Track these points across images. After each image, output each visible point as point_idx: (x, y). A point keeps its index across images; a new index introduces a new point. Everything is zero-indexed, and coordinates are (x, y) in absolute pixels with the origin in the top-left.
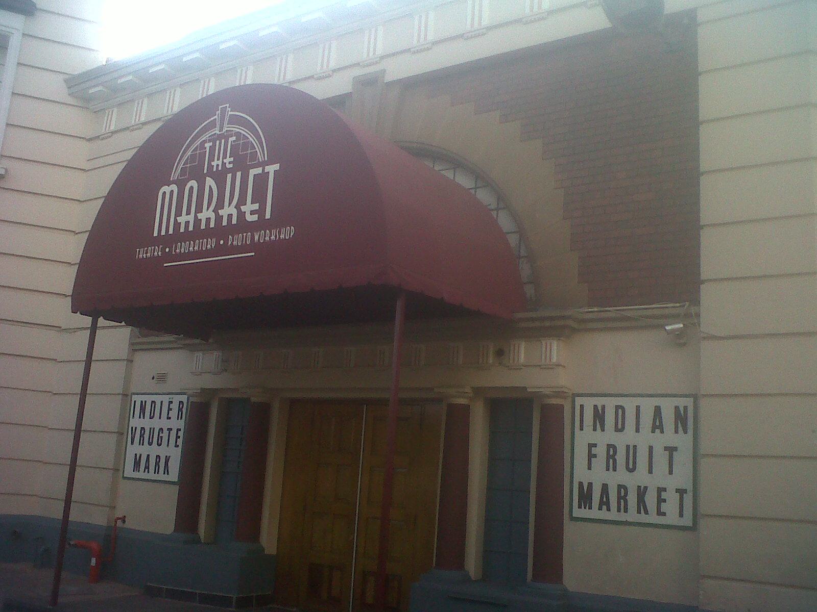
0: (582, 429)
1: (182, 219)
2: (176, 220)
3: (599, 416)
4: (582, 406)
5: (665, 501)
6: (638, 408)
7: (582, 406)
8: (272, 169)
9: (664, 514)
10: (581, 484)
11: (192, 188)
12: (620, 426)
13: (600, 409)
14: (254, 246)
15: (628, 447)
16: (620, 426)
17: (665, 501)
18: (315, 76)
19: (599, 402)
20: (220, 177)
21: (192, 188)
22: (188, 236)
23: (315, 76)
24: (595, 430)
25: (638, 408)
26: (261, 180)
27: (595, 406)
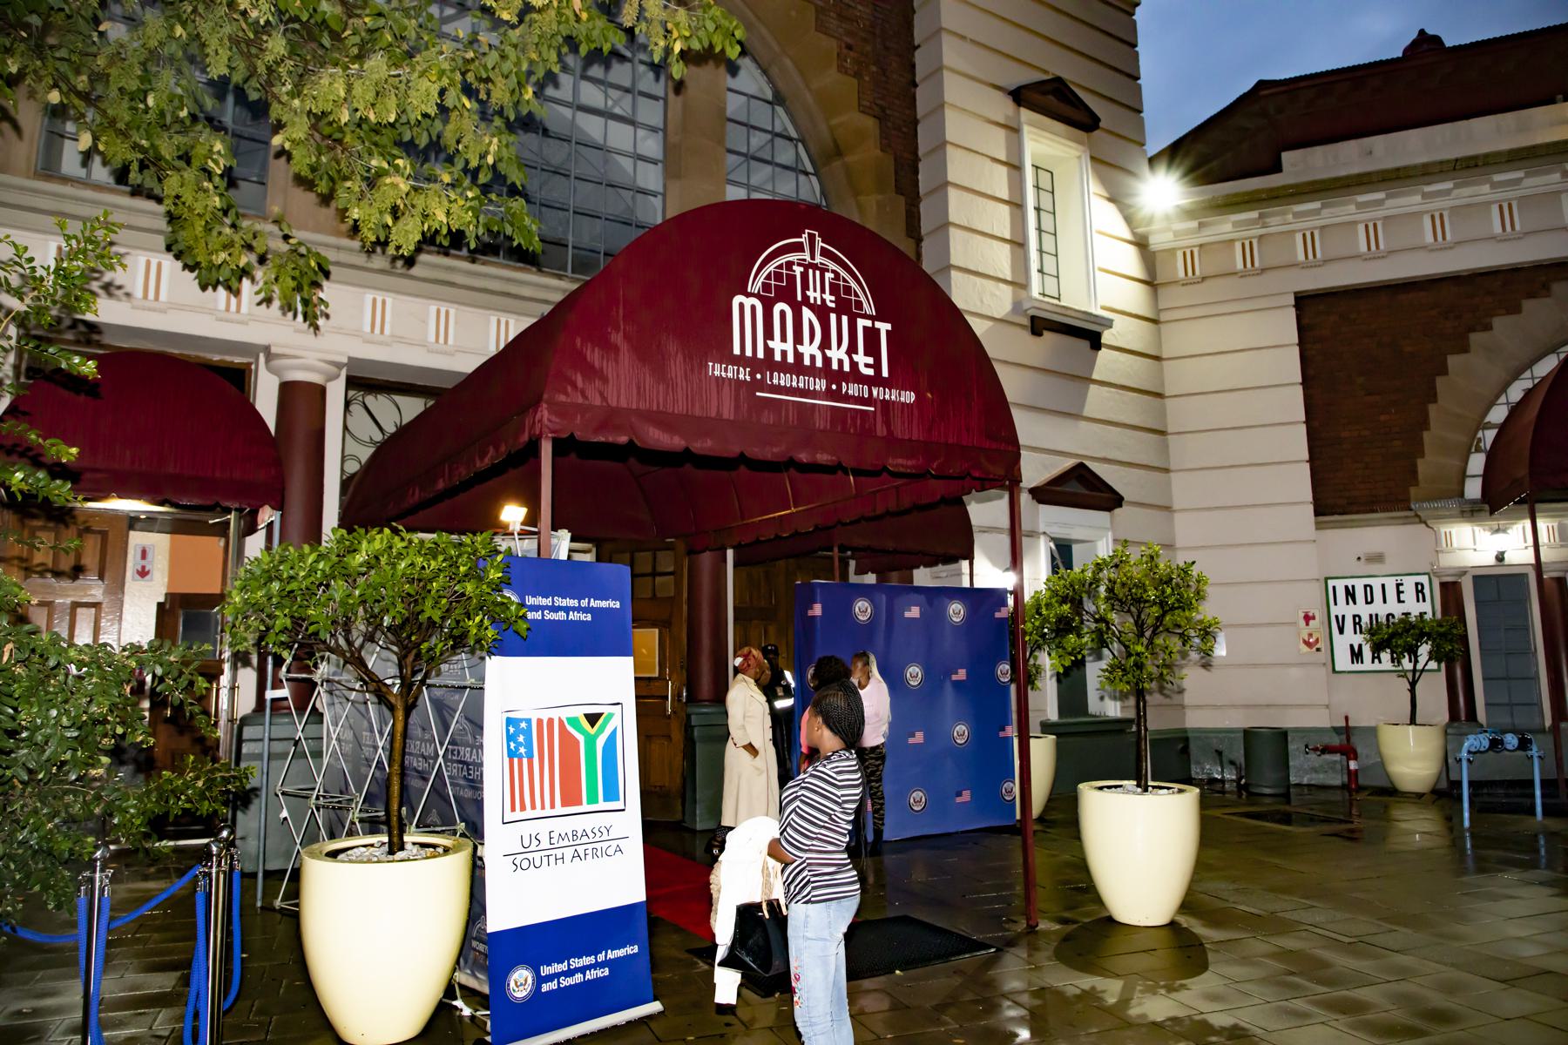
0: (1336, 604)
1: (776, 345)
2: (766, 345)
3: (1350, 594)
4: (1334, 588)
5: (1403, 592)
6: (1383, 586)
7: (1334, 588)
8: (884, 327)
9: (1403, 602)
10: (1337, 617)
11: (783, 314)
12: (1369, 600)
13: (1350, 588)
14: (869, 401)
15: (1371, 616)
16: (1369, 600)
17: (1403, 592)
18: (216, 123)
19: (1349, 583)
20: (822, 312)
21: (783, 314)
22: (783, 367)
23: (216, 123)
24: (1348, 603)
25: (1383, 586)
26: (872, 334)
27: (1347, 587)
